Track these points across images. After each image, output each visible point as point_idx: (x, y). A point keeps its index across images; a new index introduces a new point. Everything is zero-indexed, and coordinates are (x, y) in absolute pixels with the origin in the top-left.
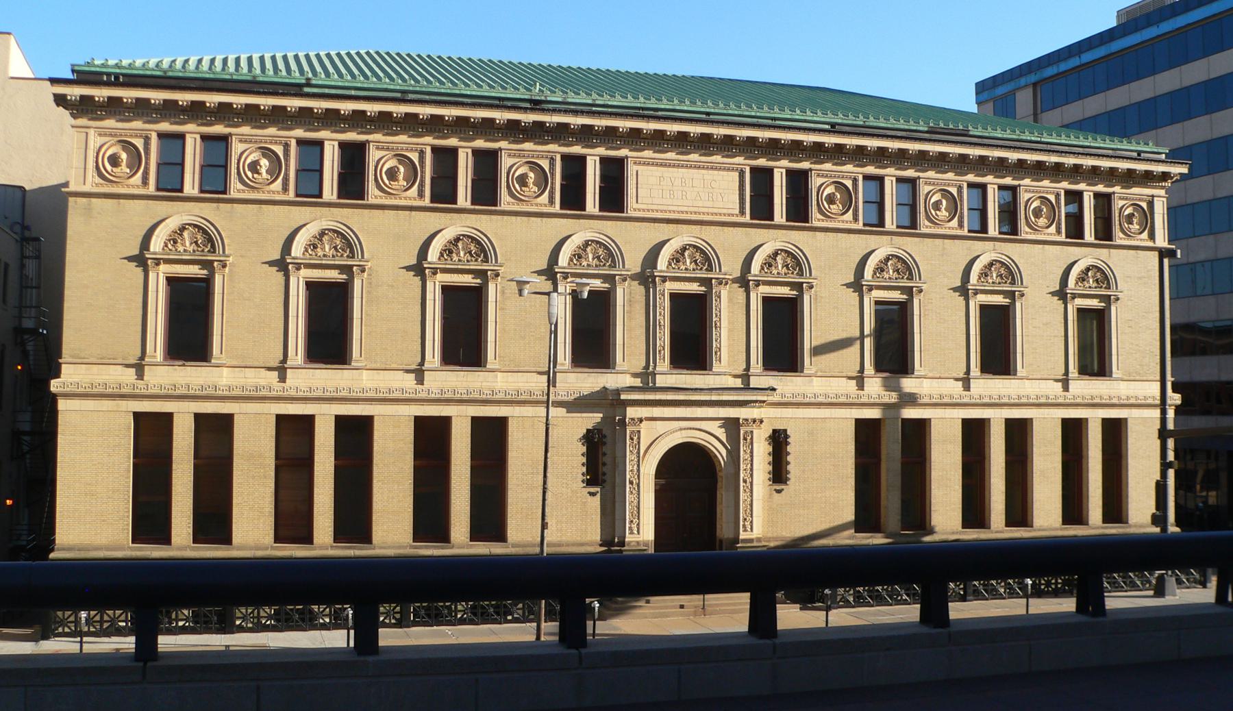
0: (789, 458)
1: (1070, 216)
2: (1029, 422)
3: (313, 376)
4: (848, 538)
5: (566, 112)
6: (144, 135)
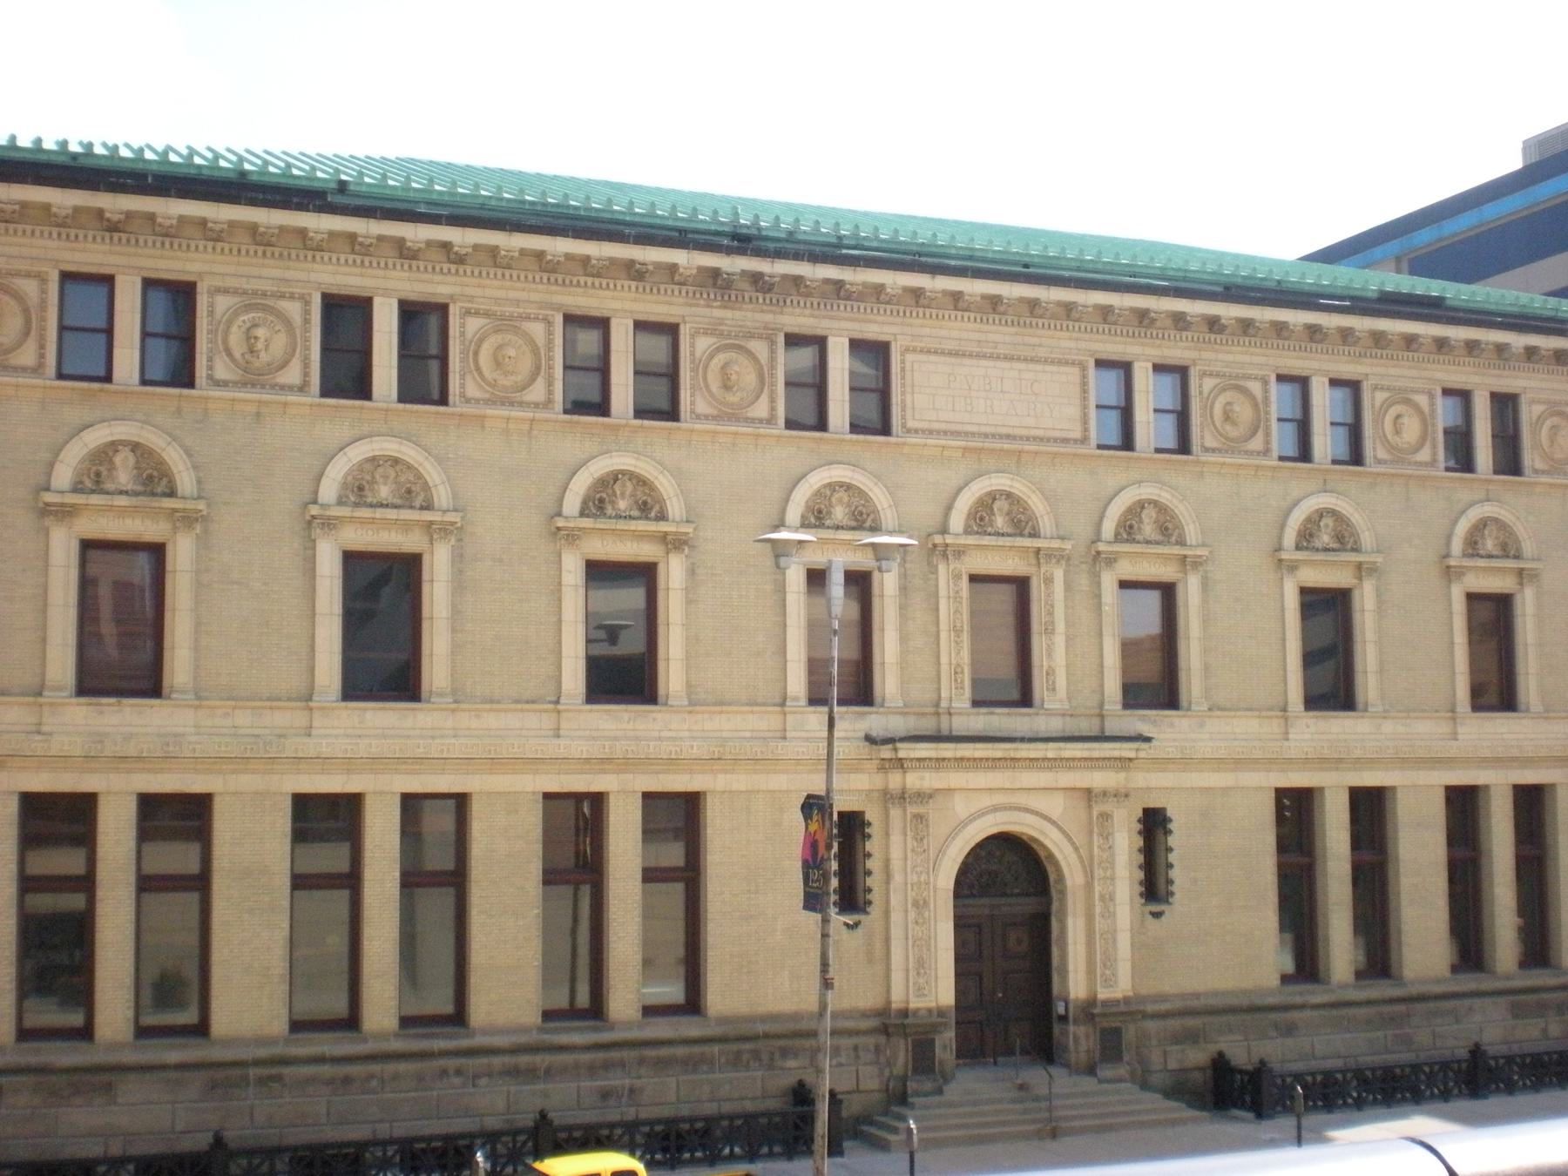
0: (1172, 858)
1: (1450, 433)
2: (1388, 795)
3: (360, 723)
4: (1054, 1015)
5: (797, 256)
6: (540, 317)
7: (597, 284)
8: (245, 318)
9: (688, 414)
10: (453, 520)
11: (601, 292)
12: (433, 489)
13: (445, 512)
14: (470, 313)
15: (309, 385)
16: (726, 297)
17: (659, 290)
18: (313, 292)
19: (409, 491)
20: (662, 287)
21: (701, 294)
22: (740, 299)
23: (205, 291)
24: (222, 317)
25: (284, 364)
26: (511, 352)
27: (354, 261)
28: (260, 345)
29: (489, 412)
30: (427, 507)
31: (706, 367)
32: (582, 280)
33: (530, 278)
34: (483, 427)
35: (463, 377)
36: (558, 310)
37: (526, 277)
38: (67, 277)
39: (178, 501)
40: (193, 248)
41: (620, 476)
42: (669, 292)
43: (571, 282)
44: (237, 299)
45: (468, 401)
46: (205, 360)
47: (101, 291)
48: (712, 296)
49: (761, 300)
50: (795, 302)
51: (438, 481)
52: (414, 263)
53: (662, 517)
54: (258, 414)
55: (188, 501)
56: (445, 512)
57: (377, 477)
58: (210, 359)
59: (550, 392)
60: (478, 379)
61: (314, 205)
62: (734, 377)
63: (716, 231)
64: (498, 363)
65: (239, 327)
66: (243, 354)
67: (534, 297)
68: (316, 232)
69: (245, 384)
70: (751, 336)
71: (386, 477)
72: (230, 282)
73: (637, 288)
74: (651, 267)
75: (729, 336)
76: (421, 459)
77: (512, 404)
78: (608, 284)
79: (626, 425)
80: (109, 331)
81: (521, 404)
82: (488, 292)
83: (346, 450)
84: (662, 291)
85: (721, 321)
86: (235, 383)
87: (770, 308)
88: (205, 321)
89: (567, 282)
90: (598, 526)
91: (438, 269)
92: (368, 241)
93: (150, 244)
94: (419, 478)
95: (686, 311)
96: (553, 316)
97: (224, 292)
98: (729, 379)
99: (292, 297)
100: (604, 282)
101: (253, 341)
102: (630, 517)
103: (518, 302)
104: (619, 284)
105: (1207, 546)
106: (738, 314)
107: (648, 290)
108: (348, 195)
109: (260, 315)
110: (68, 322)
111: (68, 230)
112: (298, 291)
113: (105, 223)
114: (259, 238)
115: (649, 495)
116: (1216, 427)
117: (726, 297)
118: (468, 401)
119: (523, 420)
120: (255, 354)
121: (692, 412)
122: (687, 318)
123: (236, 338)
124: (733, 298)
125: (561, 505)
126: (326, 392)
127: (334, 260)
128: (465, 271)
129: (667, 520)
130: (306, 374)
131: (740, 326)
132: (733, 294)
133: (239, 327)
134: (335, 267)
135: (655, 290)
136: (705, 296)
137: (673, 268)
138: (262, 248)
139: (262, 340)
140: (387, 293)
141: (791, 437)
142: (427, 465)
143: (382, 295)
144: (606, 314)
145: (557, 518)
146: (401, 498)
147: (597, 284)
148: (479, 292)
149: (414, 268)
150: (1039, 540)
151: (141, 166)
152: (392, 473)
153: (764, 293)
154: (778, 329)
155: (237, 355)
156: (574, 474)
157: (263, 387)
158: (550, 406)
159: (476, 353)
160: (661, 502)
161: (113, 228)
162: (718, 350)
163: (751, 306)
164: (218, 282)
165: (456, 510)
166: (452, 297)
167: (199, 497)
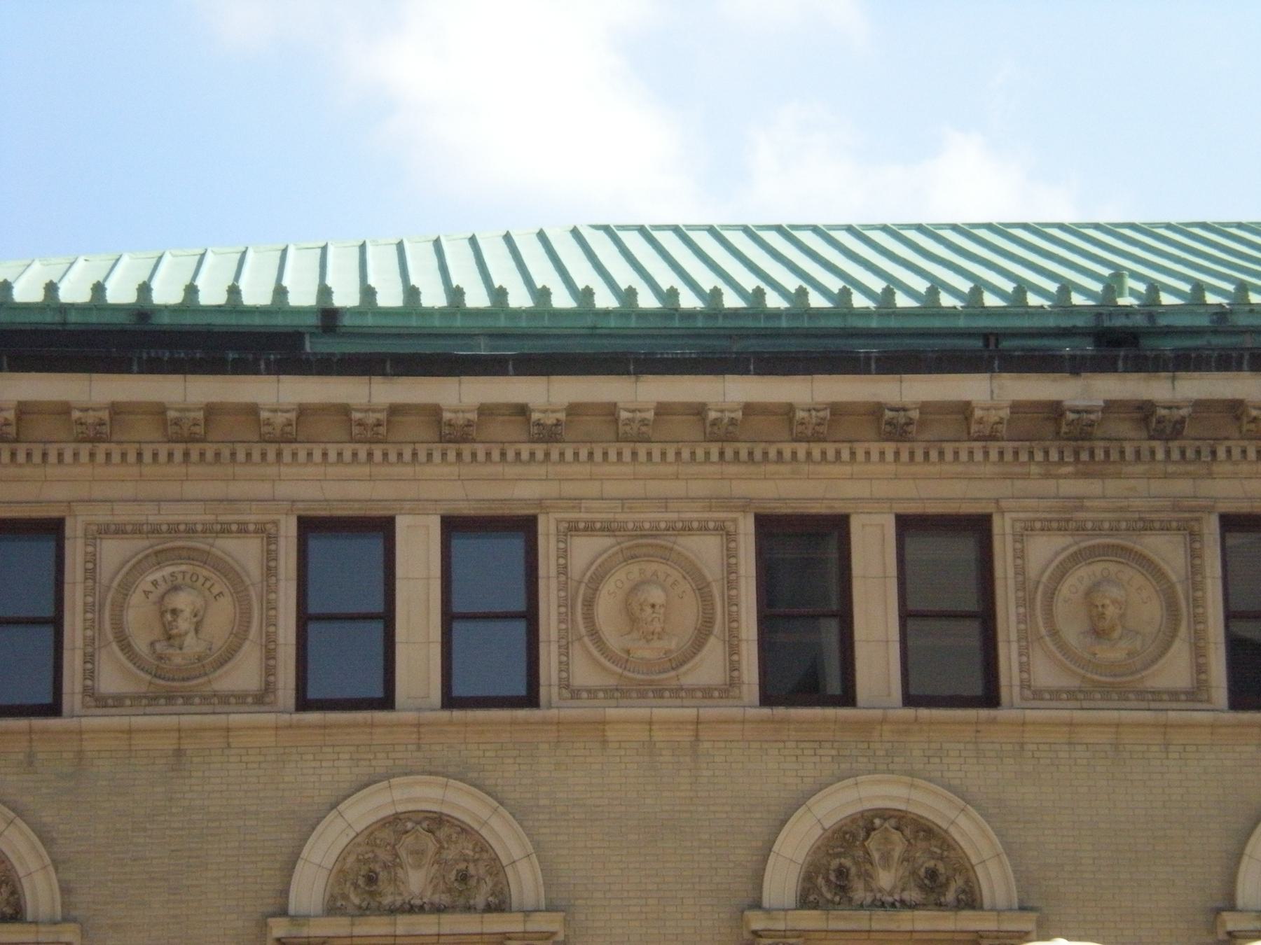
6: (711, 525)
7: (816, 454)
8: (157, 575)
9: (1016, 690)
10: (546, 927)
11: (824, 469)
12: (509, 871)
13: (527, 913)
14: (577, 529)
15: (274, 692)
16: (1084, 456)
17: (941, 454)
18: (282, 518)
19: (464, 877)
20: (949, 448)
21: (1031, 454)
22: (1114, 456)
23: (80, 533)
24: (112, 580)
25: (228, 656)
26: (656, 595)
27: (355, 455)
28: (183, 624)
29: (612, 713)
30: (499, 906)
31: (1051, 595)
32: (787, 449)
33: (686, 455)
34: (605, 742)
35: (565, 650)
36: (744, 509)
37: (678, 454)
38: (309, 526)
39: (25, 927)
40: (53, 458)
41: (877, 822)
42: (964, 456)
43: (765, 454)
44: (140, 543)
45: (575, 694)
46: (79, 656)
47: (514, 546)
48: (1054, 456)
49: (1160, 455)
50: (1236, 453)
51: (517, 853)
52: (466, 449)
53: (970, 901)
54: (179, 753)
55: (43, 929)
56: (527, 913)
57: (403, 853)
58: (89, 658)
59: (734, 667)
60: (596, 653)
61: (268, 363)
62: (1111, 611)
63: (1059, 328)
64: (632, 619)
65: (146, 593)
66: (152, 644)
67: (699, 488)
68: (1170, 408)
69: (153, 699)
70: (1146, 526)
71: (419, 853)
72: (125, 514)
73: (897, 454)
74: (915, 414)
75: (1098, 529)
76: (484, 813)
77: (659, 693)
78: (838, 453)
79: (884, 721)
80: (387, 618)
81: (677, 692)
82: (612, 489)
83: (341, 807)
84: (949, 456)
85: (1079, 502)
86: (136, 698)
87: (1182, 468)
88: (554, 584)
89: (758, 455)
90: (833, 925)
91: (511, 455)
92: (372, 418)
93: (613, 456)
94: (483, 849)
95: (1003, 488)
96: (735, 521)
97: (116, 532)
98: (1102, 616)
99: (243, 530)
100: (831, 449)
101: (169, 617)
102: (902, 902)
103: (664, 502)
104: (860, 449)
105: (1032, 909)
106: (1113, 486)
107: (919, 456)
108: (344, 335)
109: (184, 568)
110: (912, 606)
111: (294, 446)
112: (253, 518)
113: (535, 430)
114: (171, 430)
115: (941, 858)
116: (1063, 647)
117: (1084, 456)
118: (575, 694)
119: (680, 723)
120: (176, 642)
121: (1025, 685)
122: (1003, 504)
123: (138, 615)
124: (1100, 455)
125: (759, 887)
126: (767, 699)
127: (317, 456)
128: (737, 453)
129: (981, 908)
130: (270, 672)
131: (1121, 509)
132: (1100, 447)
133: (146, 593)
134: (322, 469)
135: (934, 455)
136: (1039, 456)
137: (964, 410)
138: (366, 446)
139: (187, 613)
140: (418, 507)
141: (1241, 725)
142: (495, 823)
143: (411, 512)
144: (839, 508)
145: (1225, 915)
146: (449, 891)
147: (816, 454)
148: (593, 489)
149: (467, 456)
150: (506, 916)
151: (280, 321)
152: (430, 845)
153: (1167, 440)
154: (1202, 509)
155: (141, 645)
156: (784, 822)
157: (188, 700)
158: (736, 692)
159: (589, 604)
160: (964, 868)
161: (549, 434)
162: (1077, 558)
163: (1140, 468)
164: (102, 515)
165: (551, 908)
166: (540, 502)
167: (66, 919)
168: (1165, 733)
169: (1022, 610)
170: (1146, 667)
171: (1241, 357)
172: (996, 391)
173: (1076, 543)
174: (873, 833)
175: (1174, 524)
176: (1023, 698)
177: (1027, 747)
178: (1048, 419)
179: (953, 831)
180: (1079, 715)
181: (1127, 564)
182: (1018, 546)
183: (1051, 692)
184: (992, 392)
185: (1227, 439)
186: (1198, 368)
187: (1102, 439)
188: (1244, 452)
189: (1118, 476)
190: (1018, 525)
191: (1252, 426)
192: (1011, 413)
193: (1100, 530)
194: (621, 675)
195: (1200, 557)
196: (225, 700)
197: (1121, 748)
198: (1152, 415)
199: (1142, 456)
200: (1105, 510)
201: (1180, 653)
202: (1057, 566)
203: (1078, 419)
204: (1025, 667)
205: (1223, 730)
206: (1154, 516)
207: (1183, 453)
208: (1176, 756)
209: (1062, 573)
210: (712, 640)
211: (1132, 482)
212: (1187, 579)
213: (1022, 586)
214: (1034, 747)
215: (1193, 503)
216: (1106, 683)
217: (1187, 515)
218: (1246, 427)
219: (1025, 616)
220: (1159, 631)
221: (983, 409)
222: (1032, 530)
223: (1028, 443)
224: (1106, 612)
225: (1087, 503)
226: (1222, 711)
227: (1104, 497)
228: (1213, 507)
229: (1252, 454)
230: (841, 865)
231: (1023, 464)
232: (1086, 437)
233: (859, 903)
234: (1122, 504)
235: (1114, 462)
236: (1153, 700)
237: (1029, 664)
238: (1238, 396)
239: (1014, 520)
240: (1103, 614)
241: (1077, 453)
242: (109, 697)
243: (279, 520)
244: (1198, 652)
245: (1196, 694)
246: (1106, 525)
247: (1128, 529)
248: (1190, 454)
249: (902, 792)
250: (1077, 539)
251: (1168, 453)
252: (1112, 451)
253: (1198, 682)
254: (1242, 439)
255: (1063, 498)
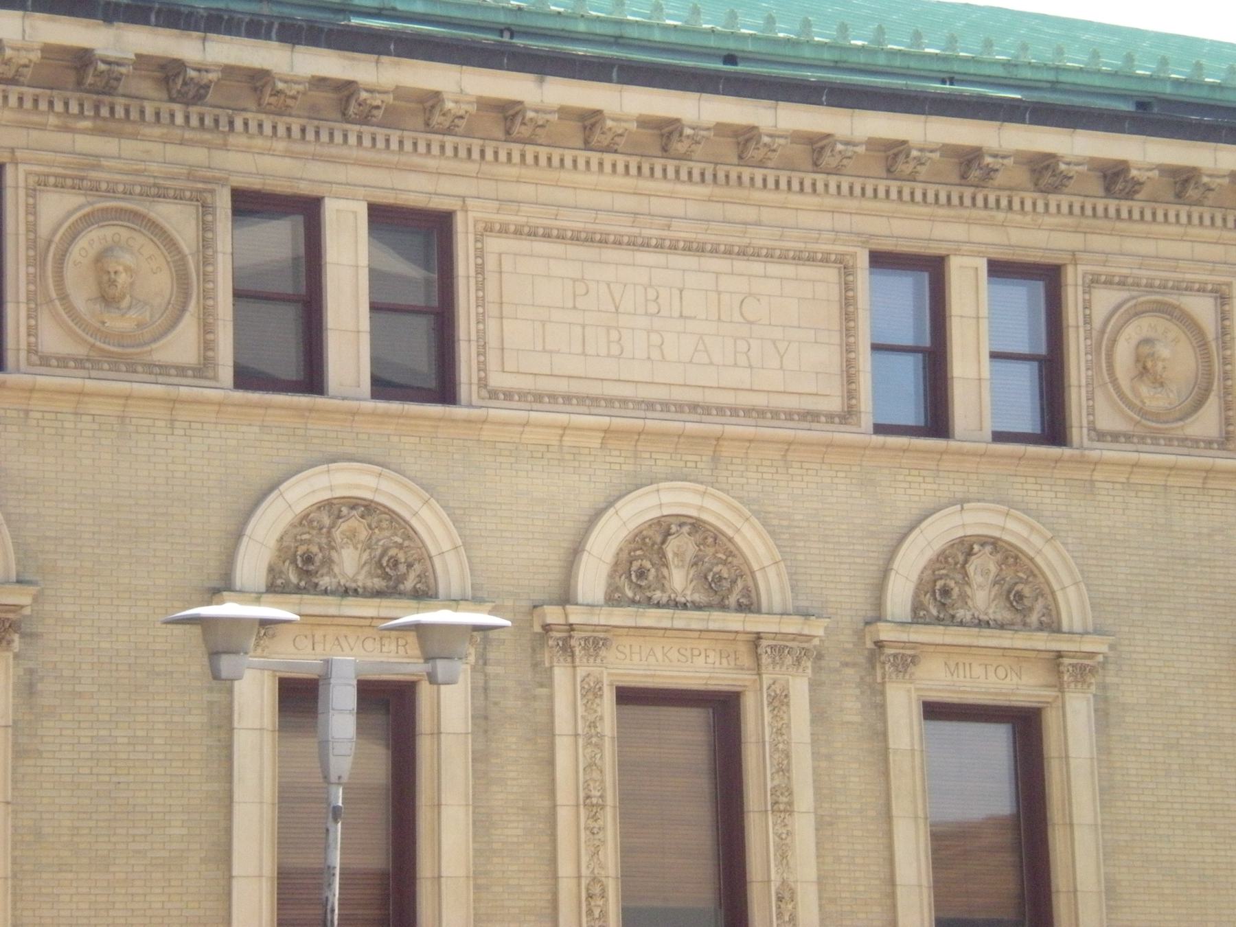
9: (23, 354)
16: (105, 112)
21: (51, 104)
22: (134, 115)
48: (74, 108)
49: (179, 119)
50: (253, 126)
51: (446, 546)
62: (122, 279)
68: (199, 70)
70: (160, 193)
75: (111, 192)
85: (94, 161)
87: (198, 135)
98: (113, 283)
106: (130, 147)
117: (105, 112)
118: (45, 361)
121: (32, 350)
124: (120, 112)
131: (137, 173)
132: (120, 103)
136: (59, 107)
162: (90, 220)
163: (157, 131)
165: (1098, 632)
168: (125, 406)
169: (32, 270)
170: (155, 340)
171: (271, 25)
172: (28, 31)
173: (90, 204)
174: (670, 538)
175: (188, 194)
176: (29, 363)
177: (32, 414)
178: (67, 67)
179: (738, 539)
180: (91, 385)
181: (140, 231)
182: (31, 201)
183: (58, 359)
184: (24, 31)
185: (244, 110)
186: (229, 32)
187: (124, 96)
188: (260, 126)
189: (134, 136)
190: (32, 180)
191: (273, 100)
192: (42, 58)
193: (114, 192)
194: (1138, 423)
195: (212, 230)
196: (162, 370)
197: (127, 421)
198: (177, 75)
199: (162, 120)
200: (121, 172)
201: (189, 327)
202: (70, 227)
203: (110, 70)
204: (32, 331)
205: (230, 409)
206: (168, 183)
207: (202, 120)
208: (182, 432)
209: (74, 235)
210: (187, 316)
211: (148, 146)
212: (198, 251)
213: (32, 244)
214: (39, 415)
215: (209, 174)
216: (113, 352)
217: (200, 186)
218: (267, 99)
219: (35, 277)
220: (169, 303)
221: (13, 48)
222: (45, 185)
223: (48, 92)
224: (118, 280)
225: (104, 162)
226: (365, 400)
227: (119, 158)
228: (227, 179)
229: (1231, 224)
230: (945, 585)
231: (42, 113)
232: (109, 90)
233: (323, 588)
234: (138, 167)
235: (337, 145)
236: (160, 374)
237: (36, 329)
238: (266, 66)
239: (28, 174)
240: (115, 281)
241: (97, 108)
242: (795, 413)
243: (1231, 283)
244: (207, 328)
245: (203, 370)
246: (121, 188)
247: (141, 194)
248: (208, 121)
249: (998, 520)
250: (90, 199)
251: (187, 118)
252: (131, 109)
253: (205, 359)
254: (258, 111)
255: (79, 154)
